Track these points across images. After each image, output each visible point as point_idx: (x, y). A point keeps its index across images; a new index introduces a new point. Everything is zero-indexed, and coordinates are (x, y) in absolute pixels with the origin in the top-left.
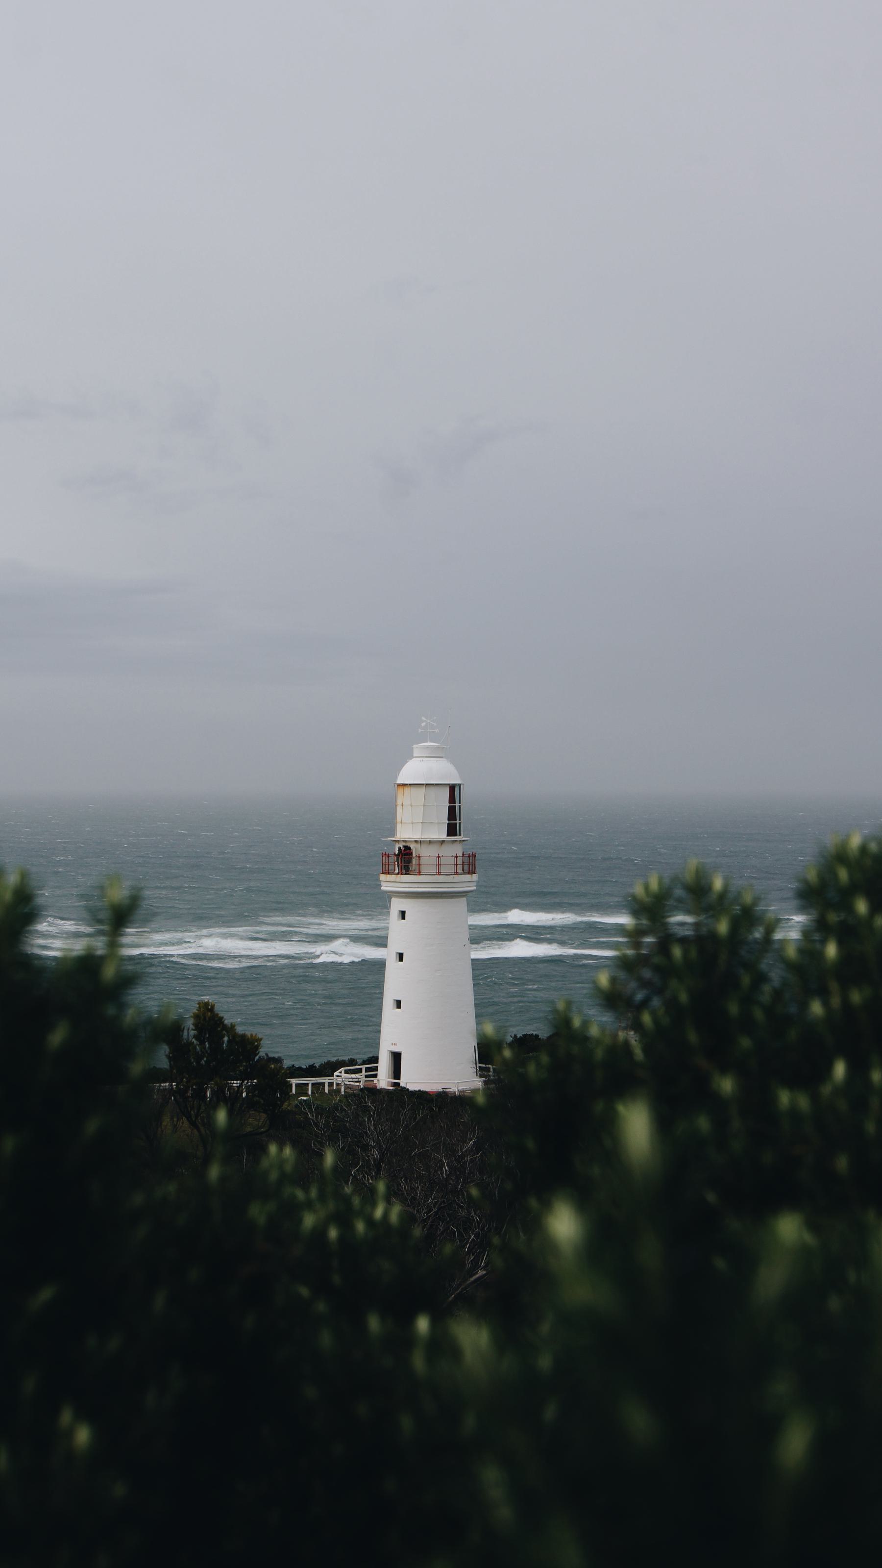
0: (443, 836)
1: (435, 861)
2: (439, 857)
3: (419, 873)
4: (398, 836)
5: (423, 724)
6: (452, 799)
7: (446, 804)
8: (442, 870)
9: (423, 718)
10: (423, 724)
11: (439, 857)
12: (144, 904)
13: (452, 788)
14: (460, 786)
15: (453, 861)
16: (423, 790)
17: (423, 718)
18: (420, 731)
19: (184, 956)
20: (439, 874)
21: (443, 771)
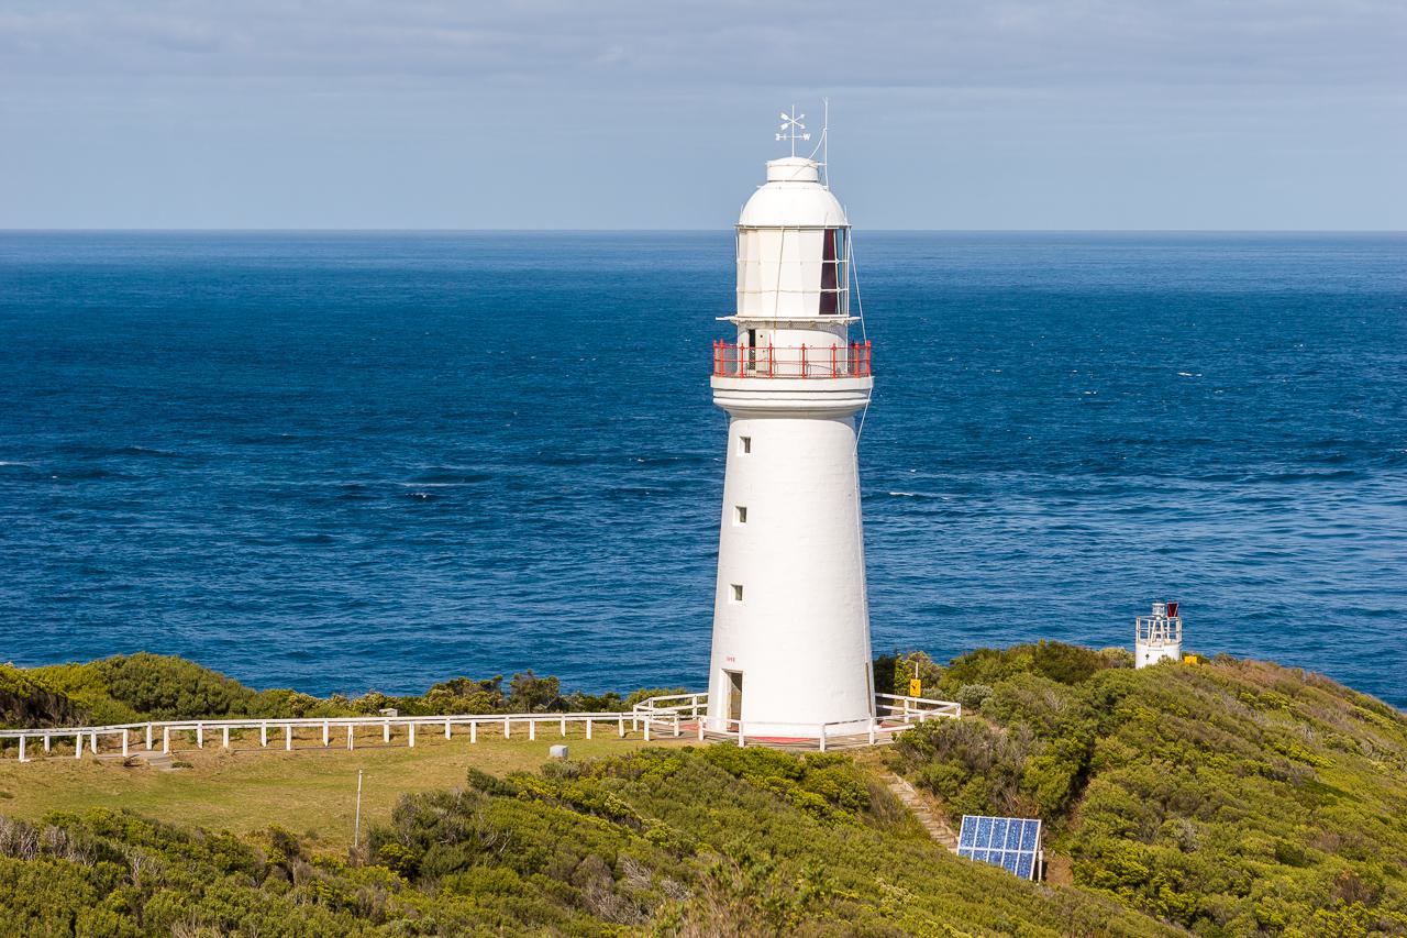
0: (812, 310)
1: (796, 356)
2: (804, 348)
3: (770, 375)
4: (739, 314)
5: (785, 126)
6: (829, 252)
7: (818, 261)
8: (813, 371)
9: (785, 117)
10: (785, 126)
11: (804, 348)
12: (289, 830)
13: (829, 234)
14: (844, 229)
15: (828, 355)
16: (779, 234)
17: (785, 117)
18: (778, 137)
19: (309, 649)
20: (804, 376)
21: (822, 208)
